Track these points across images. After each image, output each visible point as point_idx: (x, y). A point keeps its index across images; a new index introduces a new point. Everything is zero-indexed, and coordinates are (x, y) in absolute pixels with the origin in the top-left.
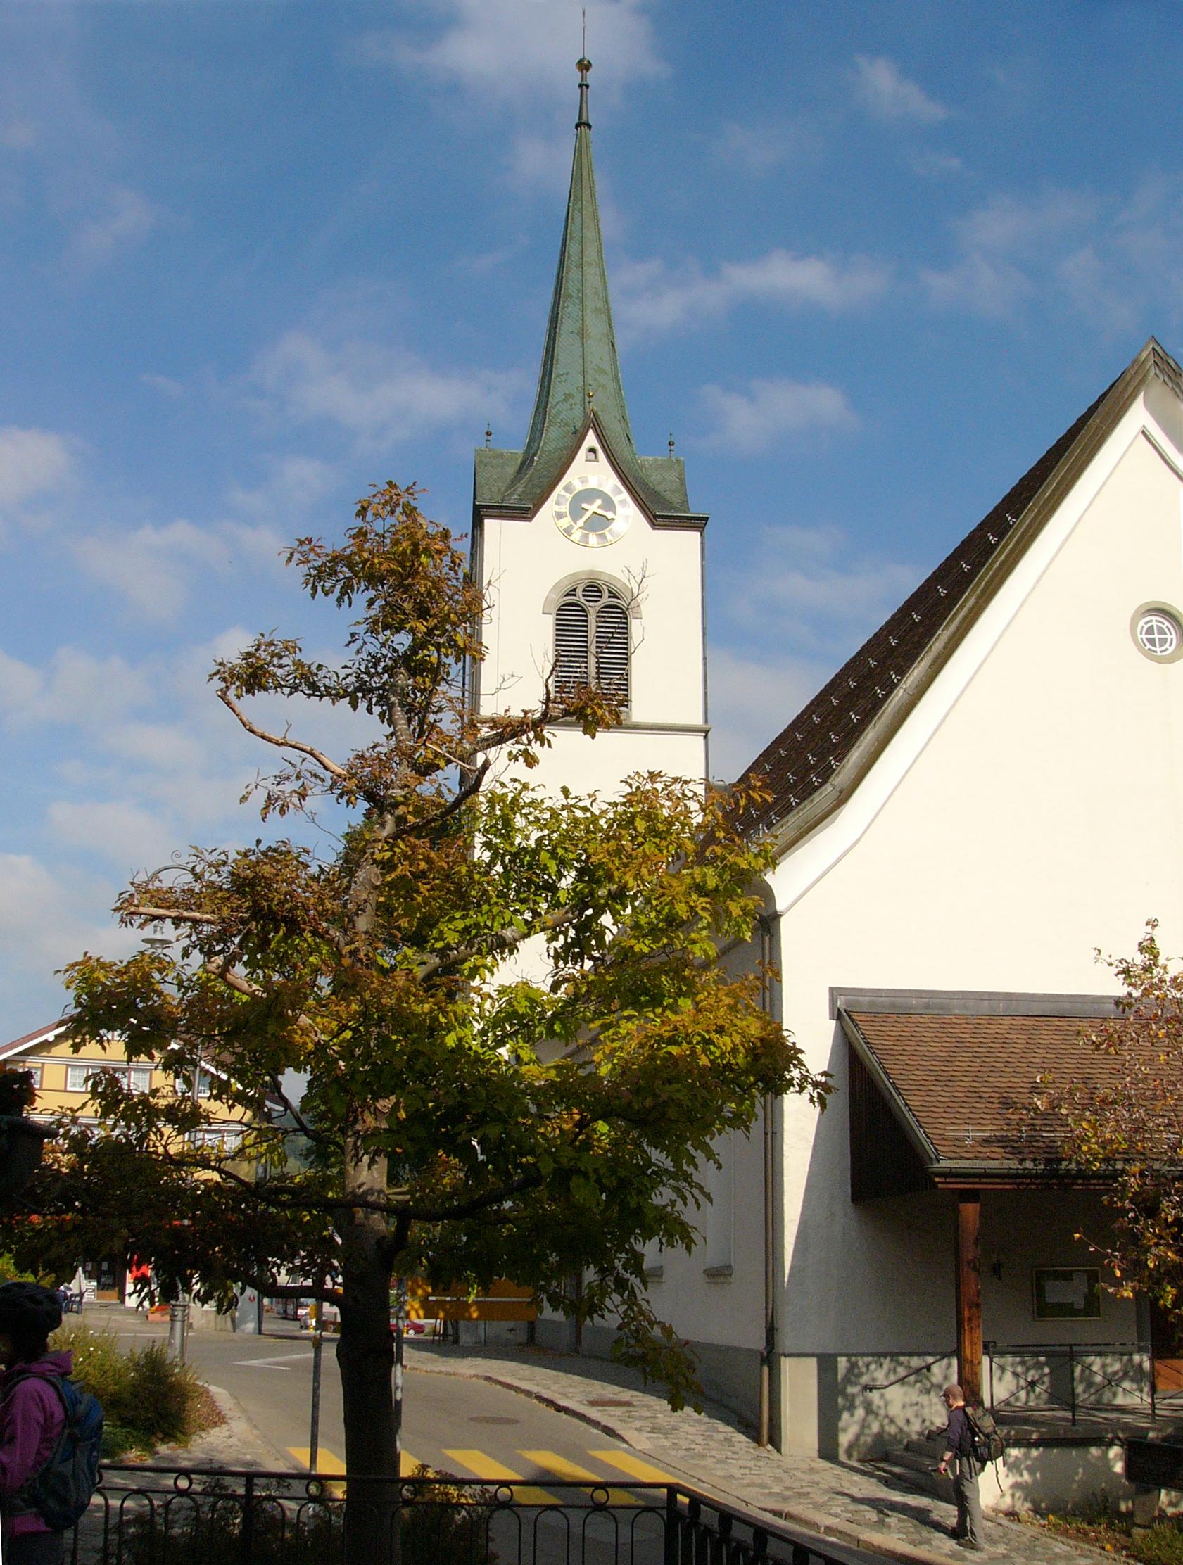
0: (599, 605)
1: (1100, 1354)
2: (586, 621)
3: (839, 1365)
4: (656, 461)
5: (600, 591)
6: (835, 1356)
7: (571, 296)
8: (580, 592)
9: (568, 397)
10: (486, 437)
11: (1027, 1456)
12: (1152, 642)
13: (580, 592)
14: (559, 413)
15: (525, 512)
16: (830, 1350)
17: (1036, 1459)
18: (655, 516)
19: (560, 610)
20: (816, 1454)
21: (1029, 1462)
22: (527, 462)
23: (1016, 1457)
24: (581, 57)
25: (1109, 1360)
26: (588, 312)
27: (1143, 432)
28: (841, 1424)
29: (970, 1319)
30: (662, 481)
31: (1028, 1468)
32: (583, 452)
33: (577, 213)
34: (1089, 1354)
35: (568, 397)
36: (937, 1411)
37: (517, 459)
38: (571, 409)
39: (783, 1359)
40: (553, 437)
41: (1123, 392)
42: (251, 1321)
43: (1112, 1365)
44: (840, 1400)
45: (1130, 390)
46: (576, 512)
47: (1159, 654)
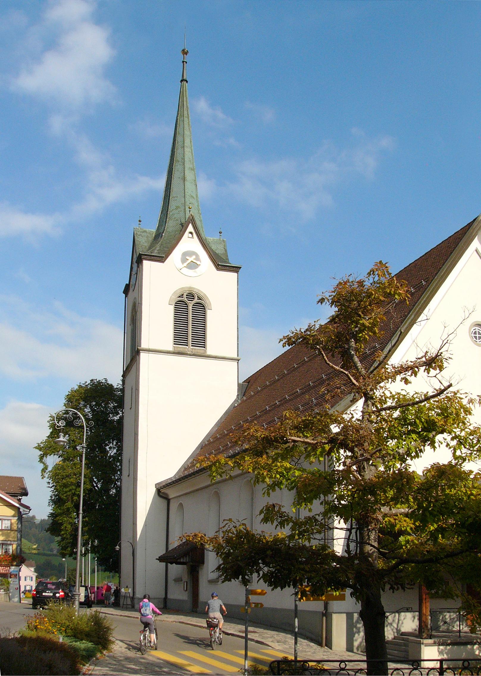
0: (193, 302)
1: (449, 612)
2: (187, 309)
3: (354, 617)
4: (214, 240)
5: (193, 296)
6: (353, 613)
7: (179, 161)
8: (185, 296)
9: (177, 207)
10: (139, 223)
11: (446, 649)
12: (476, 337)
13: (185, 296)
14: (173, 214)
15: (161, 259)
16: (351, 611)
17: (449, 650)
18: (218, 265)
19: (176, 303)
20: (345, 650)
21: (446, 651)
22: (158, 235)
23: (442, 649)
24: (183, 48)
25: (452, 614)
26: (186, 169)
27: (476, 250)
28: (354, 639)
29: (426, 599)
30: (219, 249)
31: (446, 653)
32: (187, 234)
33: (181, 123)
34: (445, 612)
35: (177, 207)
36: (390, 633)
37: (153, 234)
38: (179, 213)
39: (333, 614)
40: (171, 225)
41: (472, 233)
42: (16, 597)
43: (453, 615)
44: (354, 629)
45: (475, 232)
46: (184, 260)
47: (478, 343)
